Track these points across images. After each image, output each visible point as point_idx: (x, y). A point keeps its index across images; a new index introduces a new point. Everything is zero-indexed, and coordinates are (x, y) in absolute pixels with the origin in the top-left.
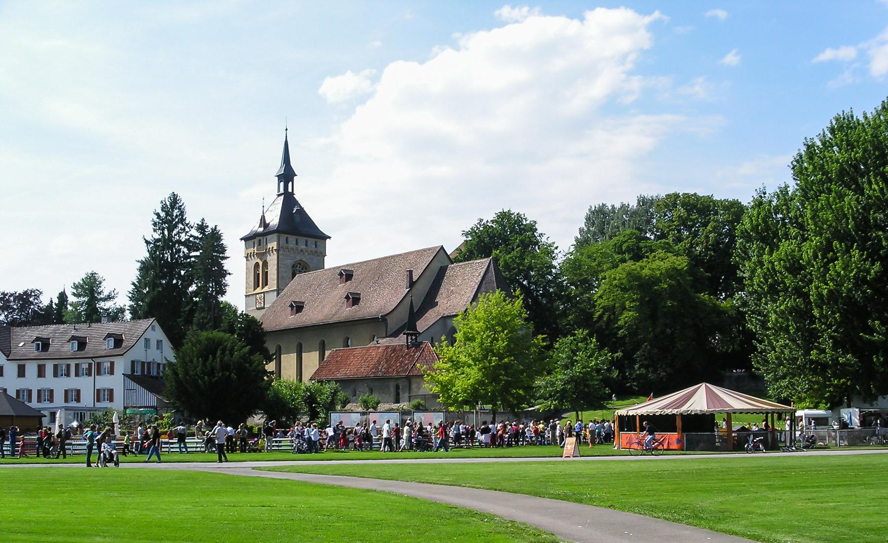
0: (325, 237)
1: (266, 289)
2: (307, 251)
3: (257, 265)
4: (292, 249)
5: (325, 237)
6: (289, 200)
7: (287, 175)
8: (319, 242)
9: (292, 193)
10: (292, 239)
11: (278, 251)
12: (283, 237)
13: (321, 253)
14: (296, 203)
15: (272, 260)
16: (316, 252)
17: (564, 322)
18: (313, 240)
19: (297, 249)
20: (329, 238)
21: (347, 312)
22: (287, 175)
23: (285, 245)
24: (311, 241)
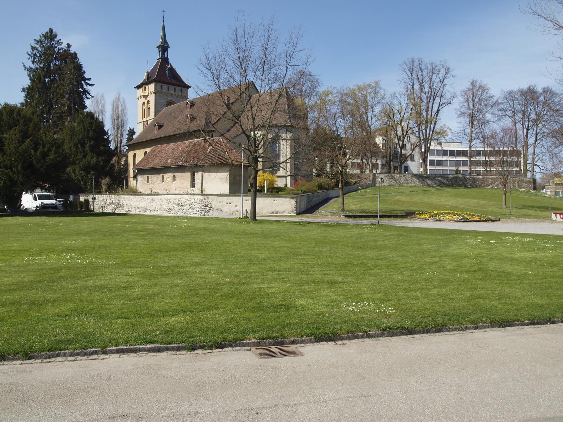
1: (149, 118)
2: (175, 95)
3: (144, 103)
4: (165, 93)
5: (188, 87)
6: (164, 61)
7: (164, 48)
8: (184, 90)
9: (167, 59)
10: (165, 86)
11: (155, 93)
12: (159, 85)
13: (185, 96)
14: (168, 63)
15: (152, 98)
16: (181, 96)
17: (69, 119)
18: (180, 88)
19: (168, 93)
20: (190, 87)
21: (176, 87)
22: (164, 48)
23: (160, 90)
24: (178, 89)
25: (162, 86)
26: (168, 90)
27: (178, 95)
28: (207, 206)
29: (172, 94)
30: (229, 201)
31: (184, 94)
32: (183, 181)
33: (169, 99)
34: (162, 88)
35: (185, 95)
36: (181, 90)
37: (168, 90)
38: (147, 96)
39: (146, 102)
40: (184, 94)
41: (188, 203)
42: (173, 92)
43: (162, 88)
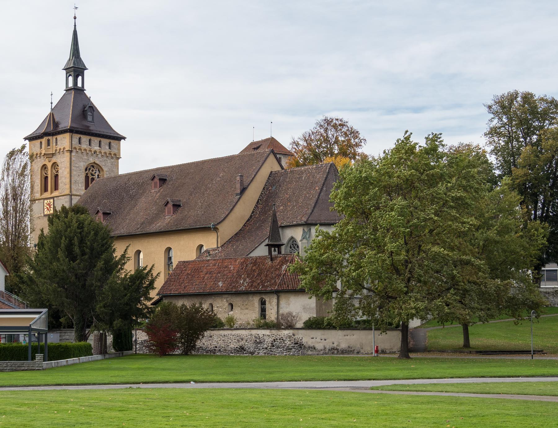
0: (119, 138)
5: (119, 138)
6: (78, 92)
7: (76, 69)
9: (82, 90)
12: (76, 137)
13: (115, 154)
18: (107, 141)
19: (90, 151)
20: (124, 138)
22: (76, 69)
24: (105, 141)
25: (80, 138)
26: (90, 145)
27: (105, 153)
28: (297, 343)
29: (95, 152)
30: (323, 337)
31: (114, 151)
32: (247, 311)
33: (91, 160)
34: (80, 143)
35: (116, 151)
36: (110, 143)
37: (90, 145)
38: (53, 154)
39: (49, 165)
40: (114, 151)
41: (269, 340)
42: (97, 148)
43: (80, 143)
